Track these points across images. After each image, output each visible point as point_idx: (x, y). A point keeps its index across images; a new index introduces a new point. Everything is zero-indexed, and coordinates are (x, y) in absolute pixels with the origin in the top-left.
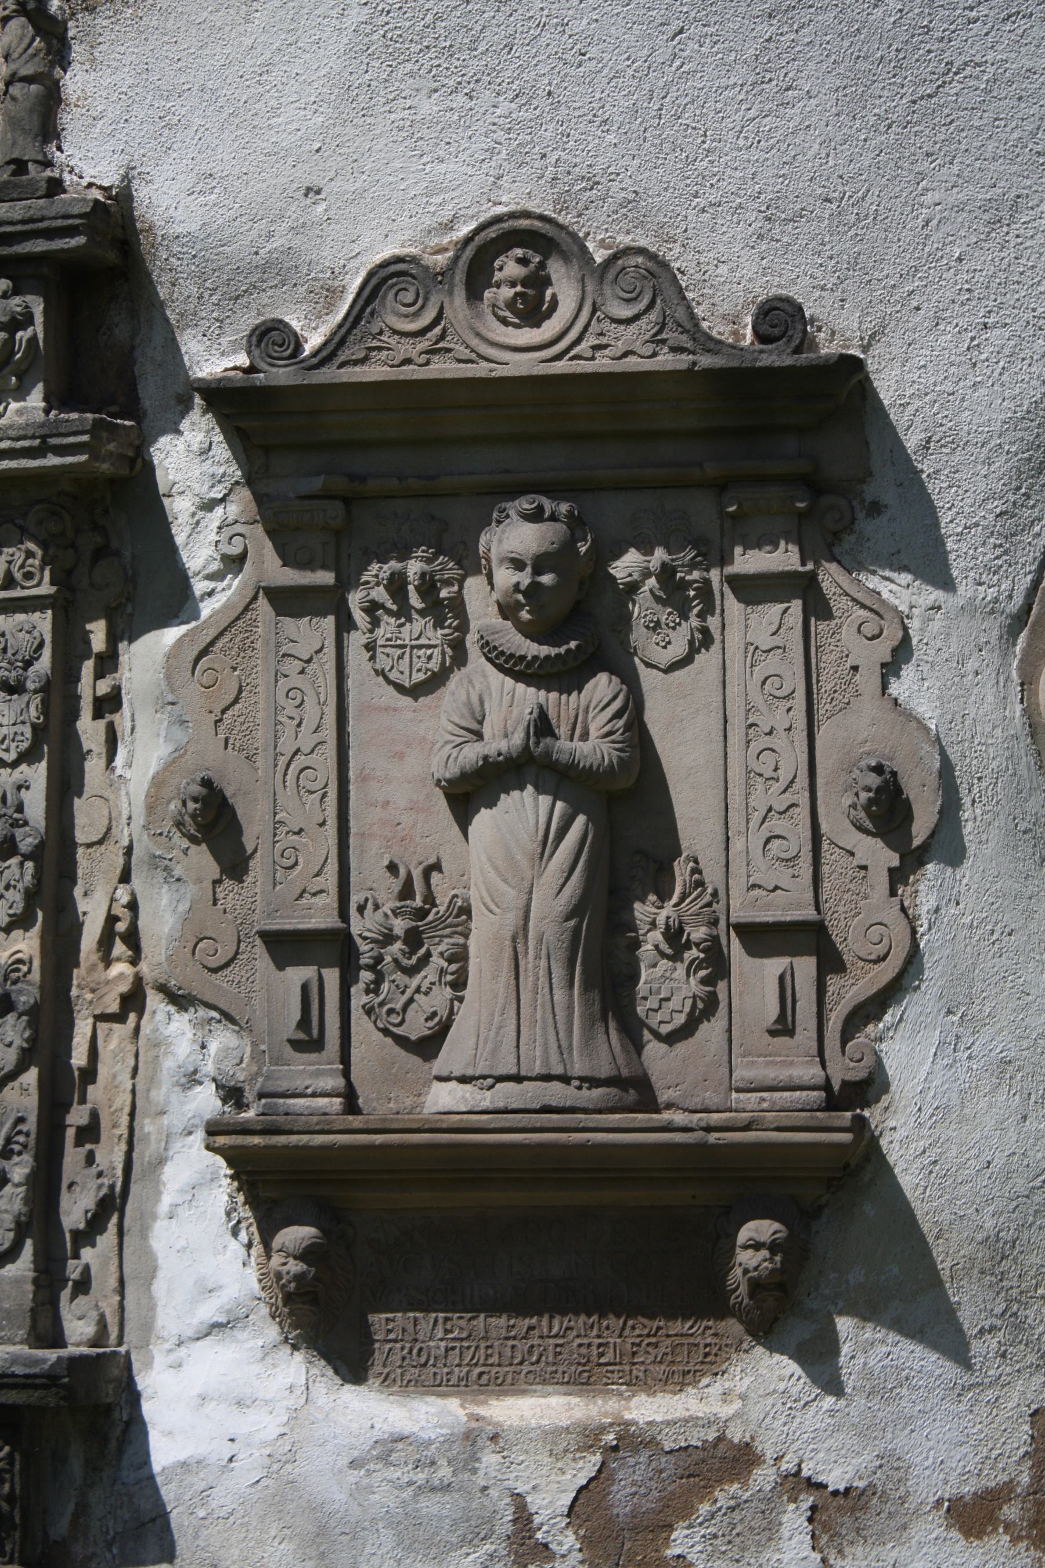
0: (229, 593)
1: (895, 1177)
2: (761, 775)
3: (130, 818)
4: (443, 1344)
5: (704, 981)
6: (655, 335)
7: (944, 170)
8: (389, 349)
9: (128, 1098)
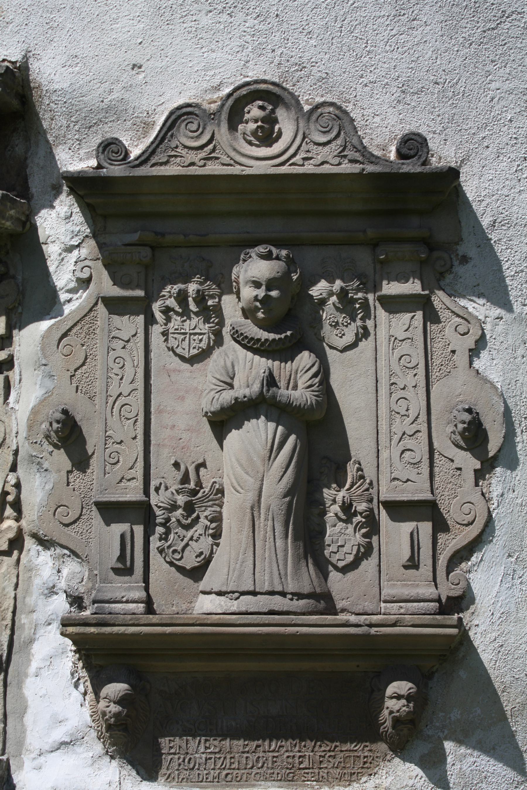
0: (80, 301)
1: (478, 654)
2: (398, 413)
3: (17, 433)
4: (204, 756)
5: (364, 536)
6: (340, 152)
7: (501, 71)
8: (181, 157)
9: (12, 602)
